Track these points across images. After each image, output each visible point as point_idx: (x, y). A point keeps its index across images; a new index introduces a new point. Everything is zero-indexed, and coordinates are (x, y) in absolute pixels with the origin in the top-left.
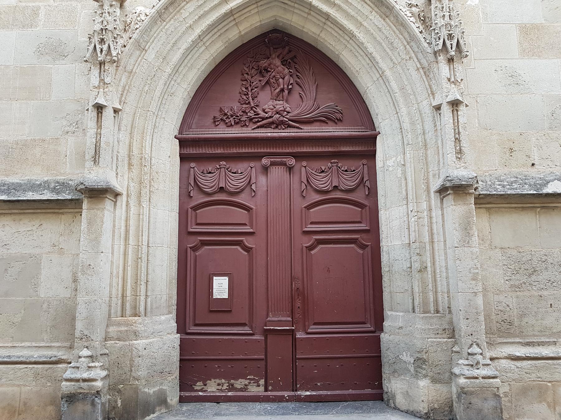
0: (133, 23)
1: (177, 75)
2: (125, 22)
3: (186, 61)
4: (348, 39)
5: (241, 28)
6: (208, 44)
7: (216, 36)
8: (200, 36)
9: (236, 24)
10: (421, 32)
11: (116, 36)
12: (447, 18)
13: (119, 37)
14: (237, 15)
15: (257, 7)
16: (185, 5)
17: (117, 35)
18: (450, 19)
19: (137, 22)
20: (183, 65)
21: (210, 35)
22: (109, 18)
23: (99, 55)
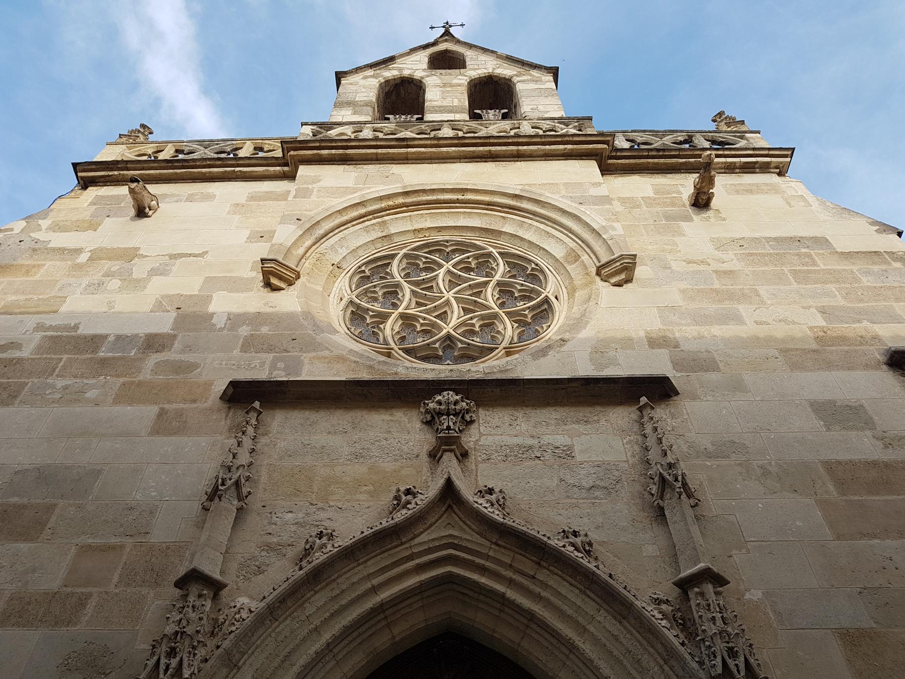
0: (227, 622)
5: (396, 631)
9: (388, 625)
10: (683, 644)
11: (195, 644)
12: (719, 622)
13: (201, 645)
14: (391, 611)
16: (313, 596)
17: (199, 642)
18: (725, 623)
19: (233, 621)
21: (346, 641)
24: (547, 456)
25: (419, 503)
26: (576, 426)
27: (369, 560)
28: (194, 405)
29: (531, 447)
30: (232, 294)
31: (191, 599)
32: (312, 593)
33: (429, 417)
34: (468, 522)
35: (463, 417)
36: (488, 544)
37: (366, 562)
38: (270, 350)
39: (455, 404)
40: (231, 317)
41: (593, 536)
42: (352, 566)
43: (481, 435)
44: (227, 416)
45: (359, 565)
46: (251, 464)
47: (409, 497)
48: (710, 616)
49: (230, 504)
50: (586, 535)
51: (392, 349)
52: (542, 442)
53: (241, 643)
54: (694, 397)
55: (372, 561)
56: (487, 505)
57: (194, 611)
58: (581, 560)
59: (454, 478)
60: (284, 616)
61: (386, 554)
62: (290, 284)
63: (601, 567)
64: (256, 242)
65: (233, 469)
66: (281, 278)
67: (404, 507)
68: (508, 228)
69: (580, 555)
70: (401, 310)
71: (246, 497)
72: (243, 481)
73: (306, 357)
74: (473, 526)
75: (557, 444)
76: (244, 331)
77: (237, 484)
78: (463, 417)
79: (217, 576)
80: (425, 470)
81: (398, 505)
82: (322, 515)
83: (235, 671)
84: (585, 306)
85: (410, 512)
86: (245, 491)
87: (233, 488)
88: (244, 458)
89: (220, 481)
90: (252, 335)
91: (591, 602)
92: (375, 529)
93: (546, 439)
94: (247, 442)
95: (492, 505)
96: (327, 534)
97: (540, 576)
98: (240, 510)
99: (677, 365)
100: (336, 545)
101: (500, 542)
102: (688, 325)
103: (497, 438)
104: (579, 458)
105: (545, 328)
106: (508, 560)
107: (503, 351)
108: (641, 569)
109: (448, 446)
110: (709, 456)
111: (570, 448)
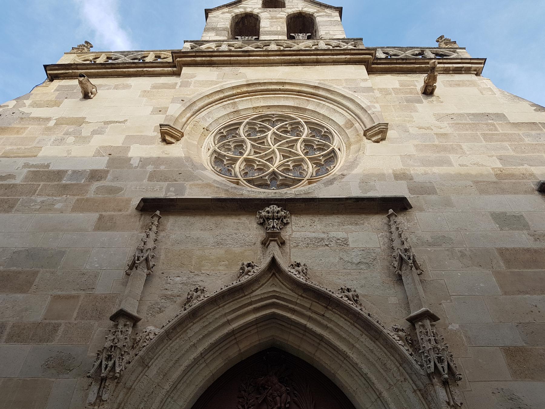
1: (174, 392)
2: (135, 340)
3: (186, 377)
4: (343, 359)
5: (241, 346)
6: (208, 361)
7: (217, 354)
8: (201, 354)
9: (237, 343)
10: (411, 355)
11: (123, 353)
12: (433, 342)
13: (126, 354)
14: (239, 335)
15: (257, 328)
16: (192, 325)
17: (125, 352)
18: (436, 343)
19: (145, 340)
20: (182, 381)
21: (212, 352)
23: (103, 371)
24: (332, 244)
25: (255, 271)
26: (350, 227)
27: (225, 305)
28: (120, 213)
30: (142, 146)
31: (120, 327)
32: (192, 324)
33: (262, 221)
34: (285, 283)
35: (282, 221)
36: (296, 296)
37: (224, 306)
38: (166, 180)
39: (277, 213)
41: (359, 292)
42: (215, 308)
43: (293, 231)
45: (220, 308)
46: (155, 248)
47: (250, 268)
48: (428, 338)
49: (142, 272)
50: (355, 291)
52: (330, 236)
53: (150, 353)
54: (421, 210)
55: (227, 306)
56: (296, 273)
58: (352, 305)
59: (276, 257)
60: (175, 337)
61: (235, 302)
63: (363, 309)
64: (156, 114)
67: (247, 274)
68: (310, 107)
69: (351, 302)
71: (152, 267)
72: (150, 258)
73: (187, 184)
74: (288, 286)
75: (339, 237)
76: (150, 168)
77: (147, 260)
78: (282, 221)
79: (135, 314)
81: (243, 272)
82: (198, 279)
83: (146, 369)
84: (357, 154)
85: (250, 277)
86: (151, 264)
87: (144, 262)
88: (150, 244)
89: (136, 258)
90: (155, 171)
91: (357, 330)
92: (229, 287)
93: (332, 234)
94: (152, 235)
95: (299, 273)
96: (201, 290)
97: (327, 315)
98: (148, 275)
99: (411, 190)
100: (206, 296)
101: (304, 295)
102: (419, 166)
104: (351, 246)
106: (308, 305)
107: (307, 181)
108: (387, 309)
109: (273, 237)
110: (430, 245)
111: (346, 240)
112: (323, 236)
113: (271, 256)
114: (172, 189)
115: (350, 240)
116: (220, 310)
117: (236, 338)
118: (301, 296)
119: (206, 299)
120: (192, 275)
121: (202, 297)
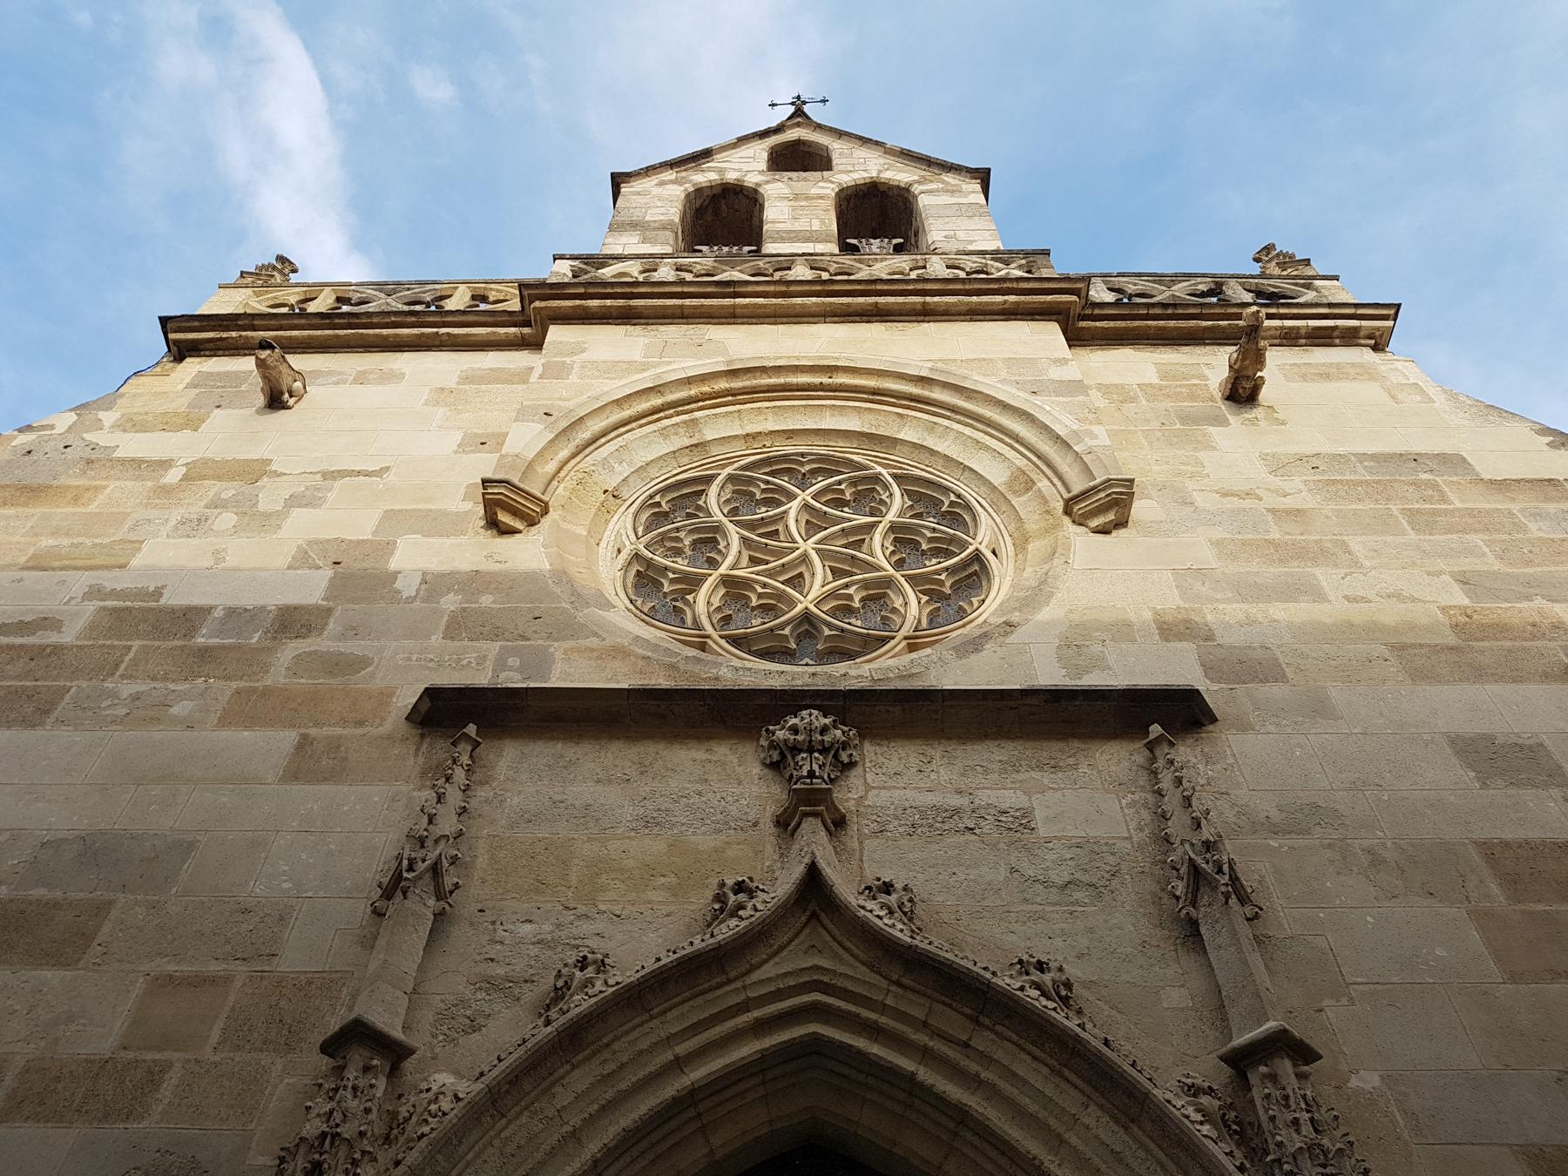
0: (414, 1118)
2: (394, 1114)
12: (1307, 1129)
13: (366, 1158)
16: (568, 1073)
17: (364, 1153)
18: (1316, 1131)
22: (353, 1104)
24: (987, 827)
25: (760, 907)
27: (670, 1009)
28: (360, 731)
29: (957, 811)
30: (430, 540)
31: (351, 1073)
32: (568, 1067)
33: (776, 756)
34: (848, 944)
36: (884, 983)
38: (495, 636)
40: (428, 578)
41: (1073, 971)
43: (868, 787)
44: (417, 750)
45: (652, 1018)
46: (460, 834)
47: (742, 897)
48: (1289, 1117)
49: (422, 906)
50: (1061, 969)
51: (708, 637)
52: (977, 802)
54: (1244, 727)
56: (882, 913)
57: (355, 1096)
58: (1053, 1014)
59: (822, 864)
60: (517, 1109)
61: (700, 1000)
62: (532, 523)
63: (1089, 1026)
65: (429, 843)
66: (515, 513)
68: (907, 434)
69: (1051, 1005)
70: (723, 570)
71: (451, 892)
72: (445, 863)
73: (558, 649)
74: (856, 951)
75: (1004, 806)
76: (450, 602)
78: (836, 756)
80: (769, 849)
81: (722, 910)
82: (586, 928)
86: (449, 881)
87: (428, 876)
88: (447, 824)
89: (405, 862)
90: (464, 610)
93: (985, 797)
94: (454, 796)
95: (891, 912)
96: (595, 962)
98: (439, 915)
99: (1209, 669)
100: (611, 982)
101: (905, 981)
103: (897, 793)
104: (1042, 832)
105: (976, 604)
107: (904, 643)
110: (1275, 830)
112: (956, 801)
113: (807, 860)
114: (513, 661)
115: (1039, 814)
116: (652, 1024)
117: (699, 1115)
118: (899, 984)
119: (611, 990)
120: (570, 916)
121: (599, 985)
